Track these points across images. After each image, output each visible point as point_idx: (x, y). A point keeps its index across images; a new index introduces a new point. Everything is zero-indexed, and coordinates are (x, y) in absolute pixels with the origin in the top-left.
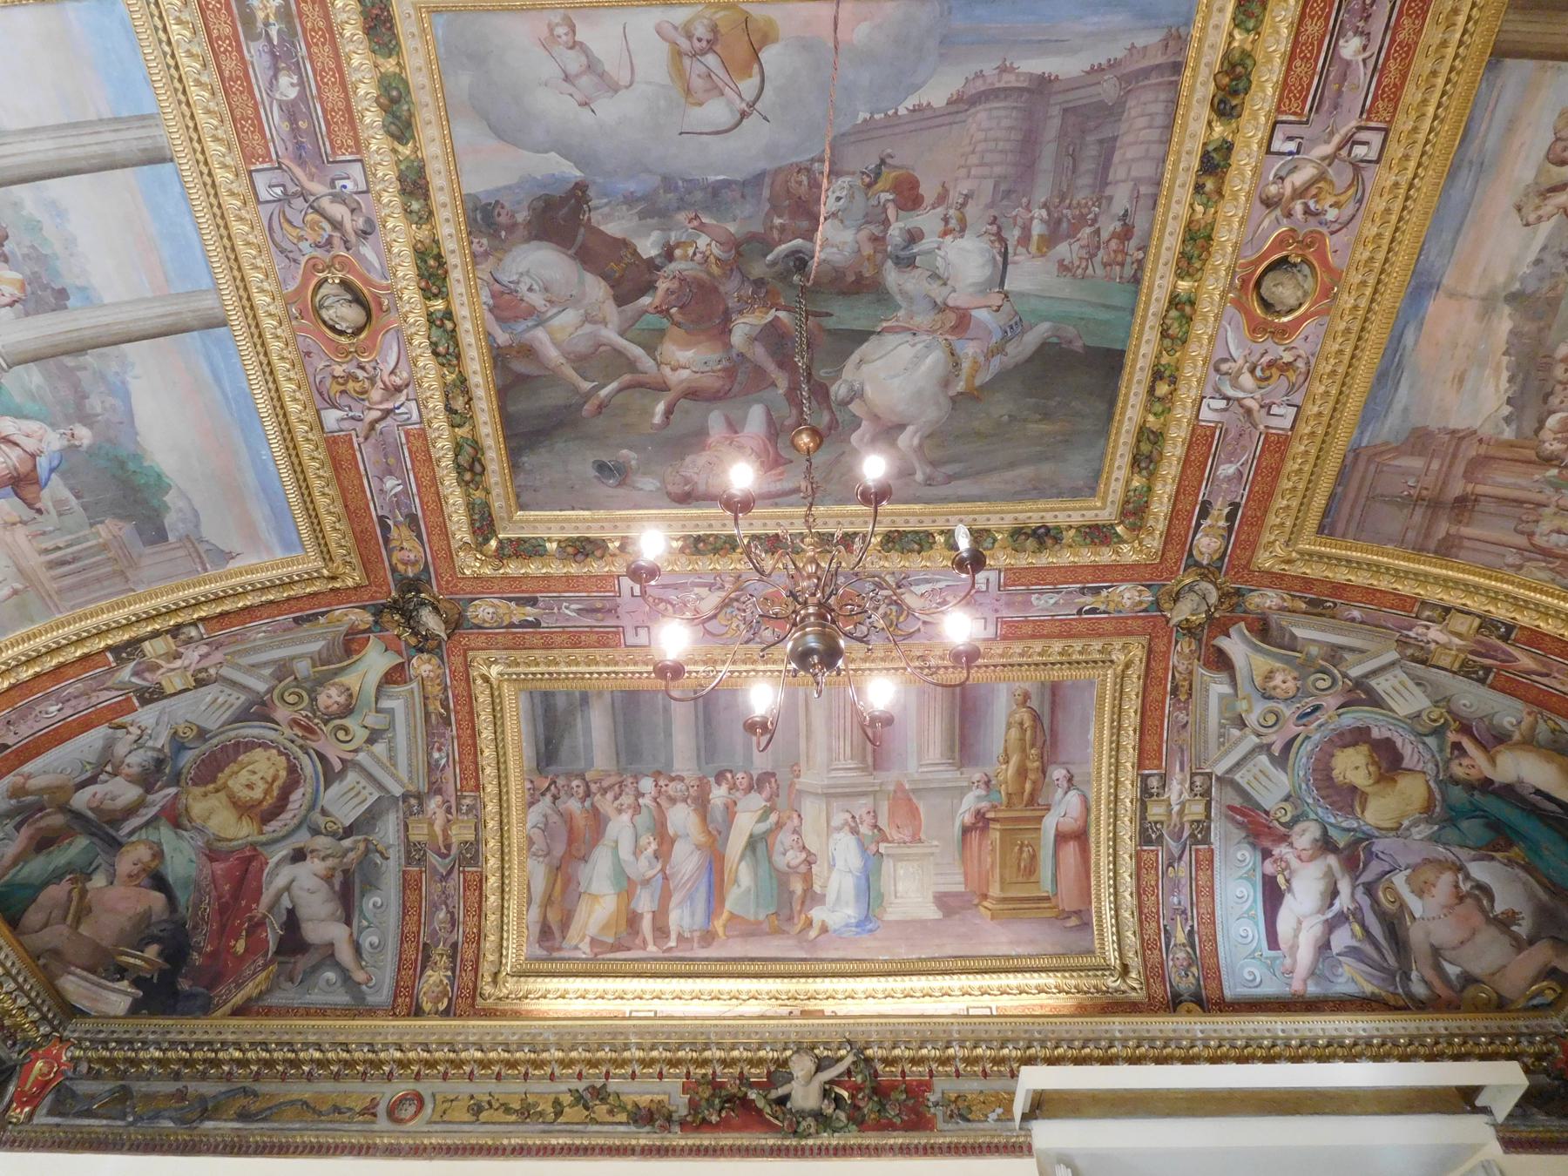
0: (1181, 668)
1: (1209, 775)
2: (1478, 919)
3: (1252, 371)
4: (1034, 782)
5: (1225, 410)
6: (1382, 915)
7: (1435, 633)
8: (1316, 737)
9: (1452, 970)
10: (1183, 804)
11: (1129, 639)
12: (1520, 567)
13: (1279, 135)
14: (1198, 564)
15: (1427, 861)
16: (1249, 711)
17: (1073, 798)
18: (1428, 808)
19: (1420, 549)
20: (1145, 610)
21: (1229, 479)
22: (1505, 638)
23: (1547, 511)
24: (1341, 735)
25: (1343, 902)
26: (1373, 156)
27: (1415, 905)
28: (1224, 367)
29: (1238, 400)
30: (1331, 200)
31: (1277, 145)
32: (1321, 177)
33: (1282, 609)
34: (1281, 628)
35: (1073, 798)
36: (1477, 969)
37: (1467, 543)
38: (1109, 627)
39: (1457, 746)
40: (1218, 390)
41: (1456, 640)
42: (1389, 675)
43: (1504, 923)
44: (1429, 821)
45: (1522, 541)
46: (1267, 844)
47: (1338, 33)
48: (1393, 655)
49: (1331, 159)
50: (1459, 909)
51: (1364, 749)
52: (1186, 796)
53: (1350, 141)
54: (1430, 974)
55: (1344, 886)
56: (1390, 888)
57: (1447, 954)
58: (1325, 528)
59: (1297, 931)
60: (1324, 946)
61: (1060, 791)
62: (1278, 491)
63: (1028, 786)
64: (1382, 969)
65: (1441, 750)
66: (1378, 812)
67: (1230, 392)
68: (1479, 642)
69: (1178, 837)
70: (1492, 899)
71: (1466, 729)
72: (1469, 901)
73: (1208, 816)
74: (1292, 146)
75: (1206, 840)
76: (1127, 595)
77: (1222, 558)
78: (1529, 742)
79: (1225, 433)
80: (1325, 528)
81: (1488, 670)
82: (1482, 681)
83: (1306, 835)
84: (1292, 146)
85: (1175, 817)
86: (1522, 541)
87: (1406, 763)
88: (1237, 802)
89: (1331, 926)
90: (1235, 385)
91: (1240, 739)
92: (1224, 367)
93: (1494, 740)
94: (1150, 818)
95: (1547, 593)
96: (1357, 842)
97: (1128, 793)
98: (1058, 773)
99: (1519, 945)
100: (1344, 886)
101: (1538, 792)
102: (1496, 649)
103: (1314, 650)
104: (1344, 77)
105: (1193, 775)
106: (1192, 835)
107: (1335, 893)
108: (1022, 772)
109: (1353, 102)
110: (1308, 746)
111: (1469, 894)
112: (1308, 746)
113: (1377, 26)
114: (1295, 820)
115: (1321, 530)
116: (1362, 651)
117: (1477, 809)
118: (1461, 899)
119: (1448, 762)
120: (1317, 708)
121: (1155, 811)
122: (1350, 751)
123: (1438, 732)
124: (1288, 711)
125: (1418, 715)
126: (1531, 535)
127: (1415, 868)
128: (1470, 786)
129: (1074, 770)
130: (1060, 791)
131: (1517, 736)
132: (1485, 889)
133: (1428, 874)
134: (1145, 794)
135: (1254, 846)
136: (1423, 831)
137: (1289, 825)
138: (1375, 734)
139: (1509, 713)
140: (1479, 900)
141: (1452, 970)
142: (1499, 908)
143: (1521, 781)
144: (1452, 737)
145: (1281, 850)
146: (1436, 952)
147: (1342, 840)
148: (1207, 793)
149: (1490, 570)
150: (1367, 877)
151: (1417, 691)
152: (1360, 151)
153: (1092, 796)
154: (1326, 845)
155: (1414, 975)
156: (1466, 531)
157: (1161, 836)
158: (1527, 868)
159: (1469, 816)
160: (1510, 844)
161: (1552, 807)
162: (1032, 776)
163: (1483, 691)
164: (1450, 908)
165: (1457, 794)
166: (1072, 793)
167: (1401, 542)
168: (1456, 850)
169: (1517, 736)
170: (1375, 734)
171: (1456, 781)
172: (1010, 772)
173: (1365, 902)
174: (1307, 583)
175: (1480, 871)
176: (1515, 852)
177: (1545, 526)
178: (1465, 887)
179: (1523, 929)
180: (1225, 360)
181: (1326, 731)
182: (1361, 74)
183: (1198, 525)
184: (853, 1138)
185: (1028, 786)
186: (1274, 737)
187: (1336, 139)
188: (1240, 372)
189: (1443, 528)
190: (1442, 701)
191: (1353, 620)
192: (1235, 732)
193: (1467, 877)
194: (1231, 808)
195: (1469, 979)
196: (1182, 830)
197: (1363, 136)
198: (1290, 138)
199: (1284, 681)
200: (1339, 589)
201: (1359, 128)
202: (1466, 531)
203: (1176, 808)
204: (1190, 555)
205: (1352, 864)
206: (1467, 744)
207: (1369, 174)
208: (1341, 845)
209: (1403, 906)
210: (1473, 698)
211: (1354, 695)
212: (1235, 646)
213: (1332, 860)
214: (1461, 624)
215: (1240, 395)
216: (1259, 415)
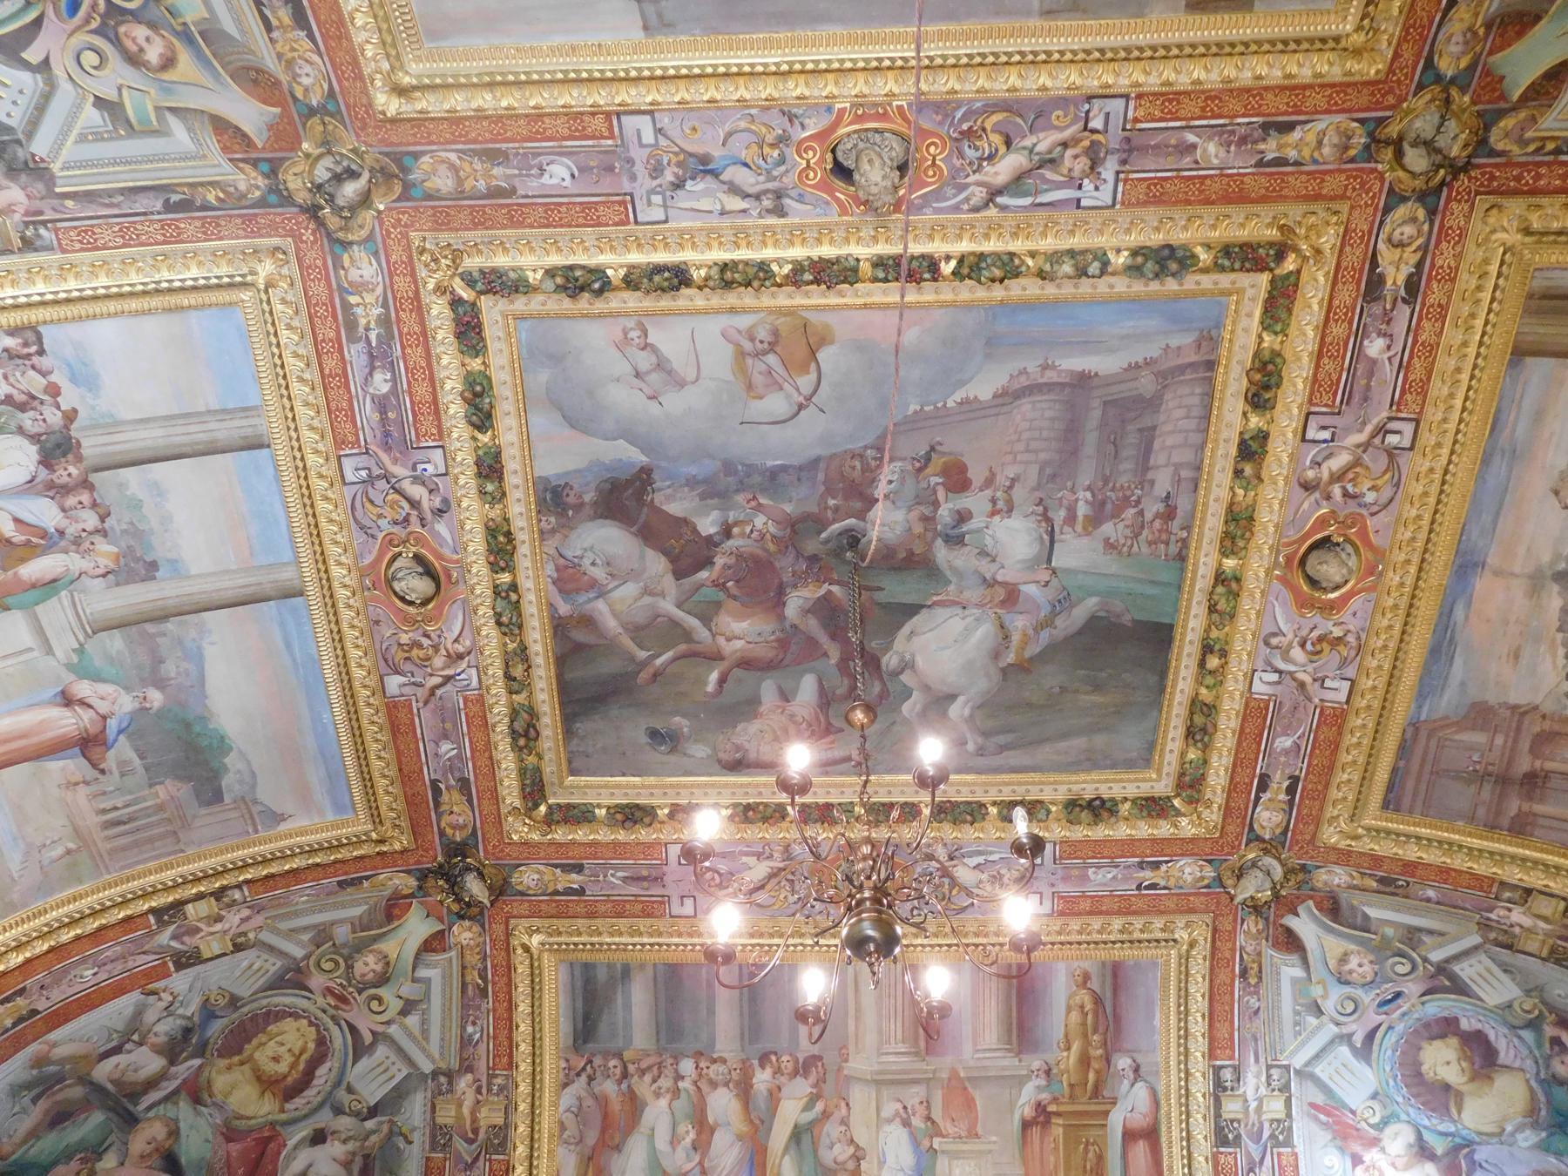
1: (1287, 1068)
3: (1303, 645)
4: (1097, 1072)
5: (1279, 683)
8: (1400, 1028)
10: (1260, 1100)
21: (1286, 752)
24: (1427, 1025)
26: (1406, 443)
28: (1274, 641)
29: (1291, 673)
32: (1357, 462)
34: (1353, 908)
37: (1541, 821)
40: (1269, 664)
41: (1542, 924)
42: (1473, 961)
44: (1535, 1125)
46: (1356, 1147)
47: (1361, 334)
48: (1476, 939)
49: (1366, 446)
52: (1263, 1090)
53: (1382, 431)
63: (1091, 1076)
67: (1282, 666)
73: (1289, 1115)
74: (1326, 435)
75: (1288, 1143)
76: (1188, 870)
79: (1279, 705)
84: (1326, 435)
85: (1253, 1117)
90: (1286, 657)
94: (1225, 1116)
96: (1456, 1149)
98: (1123, 1062)
104: (1370, 374)
105: (1269, 1067)
106: (1272, 1136)
110: (1392, 1038)
112: (1392, 1038)
113: (1400, 326)
115: (1386, 805)
116: (1442, 934)
120: (1398, 995)
121: (1231, 1108)
124: (1368, 998)
129: (1140, 1059)
135: (1342, 1150)
138: (1465, 1025)
148: (1285, 1088)
152: (1392, 439)
153: (1161, 1089)
156: (1539, 808)
157: (1238, 1137)
162: (1095, 1065)
166: (1139, 1085)
167: (1471, 819)
172: (1072, 1060)
180: (1274, 635)
181: (1410, 1021)
183: (1258, 799)
185: (1091, 1076)
186: (1354, 1027)
187: (1369, 428)
188: (1290, 646)
191: (1428, 900)
194: (1313, 1106)
197: (1393, 425)
198: (1324, 428)
199: (1360, 965)
200: (1410, 867)
201: (1390, 419)
202: (1539, 808)
203: (1253, 1105)
207: (1403, 459)
208: (1439, 1152)
212: (1304, 925)
215: (1292, 668)
216: (1314, 688)
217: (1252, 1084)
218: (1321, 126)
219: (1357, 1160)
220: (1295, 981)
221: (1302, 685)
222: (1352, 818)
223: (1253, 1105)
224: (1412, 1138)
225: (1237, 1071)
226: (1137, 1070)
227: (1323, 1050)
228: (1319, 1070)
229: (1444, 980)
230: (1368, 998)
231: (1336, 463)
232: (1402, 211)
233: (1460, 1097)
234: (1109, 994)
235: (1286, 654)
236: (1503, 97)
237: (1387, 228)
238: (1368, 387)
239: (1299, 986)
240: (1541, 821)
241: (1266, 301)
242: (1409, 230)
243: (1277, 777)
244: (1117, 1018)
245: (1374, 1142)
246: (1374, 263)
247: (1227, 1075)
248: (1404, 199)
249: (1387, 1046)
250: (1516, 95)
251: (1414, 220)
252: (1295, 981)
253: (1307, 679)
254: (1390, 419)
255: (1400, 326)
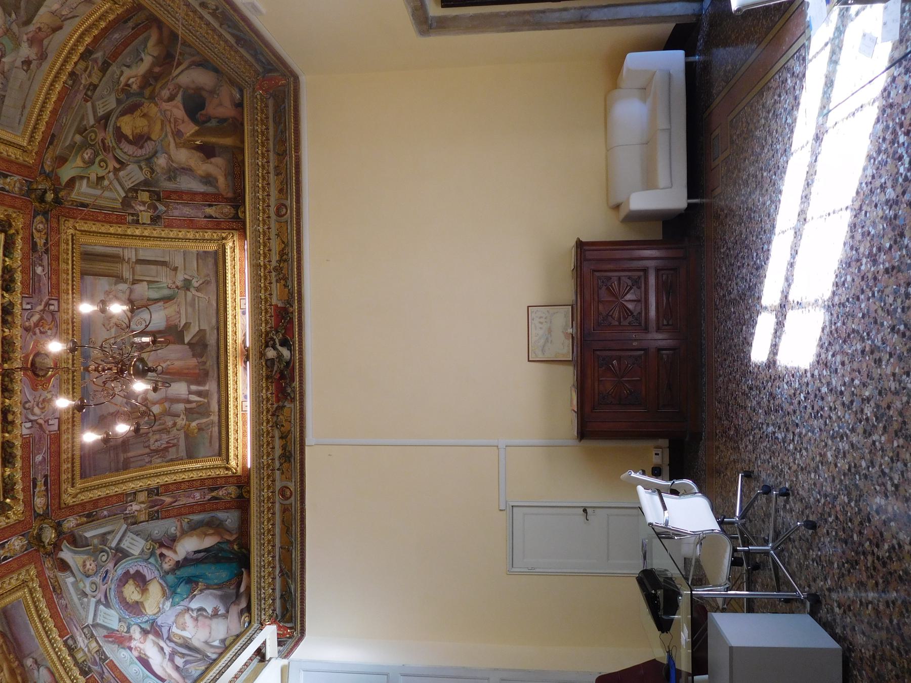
0: (52, 576)
1: (88, 626)
2: (207, 621)
3: (38, 405)
4: (21, 675)
5: (31, 427)
6: (181, 645)
7: (135, 507)
8: (113, 587)
9: (216, 643)
10: (87, 646)
11: (27, 568)
12: (151, 462)
13: (24, 303)
14: (39, 515)
15: (177, 616)
16: (85, 587)
17: (43, 671)
18: (164, 594)
19: (117, 470)
20: (26, 550)
21: (40, 463)
22: (157, 494)
23: (150, 435)
24: (120, 580)
25: (167, 650)
26: (56, 309)
27: (186, 634)
28: (27, 406)
29: (36, 421)
30: (47, 327)
31: (25, 306)
32: (41, 319)
33: (78, 525)
34: (81, 536)
35: (43, 671)
36: (222, 636)
37: (132, 460)
38: (15, 566)
39: (162, 555)
40: (27, 418)
41: (143, 506)
42: (126, 538)
43: (215, 614)
44: (167, 599)
45: (147, 450)
46: (127, 644)
47: (34, 265)
48: (125, 526)
49: (43, 311)
50: (199, 624)
51: (131, 582)
52: (86, 641)
53: (48, 304)
54: (213, 650)
55: (162, 644)
56: (175, 634)
57: (210, 640)
58: (83, 476)
59: (164, 669)
60: (177, 668)
61: (36, 672)
62: (62, 461)
63: (19, 678)
64: (200, 660)
65: (157, 561)
66: (150, 608)
67: (32, 418)
68: (150, 502)
69: (95, 663)
70: (205, 610)
71: (162, 545)
72: (200, 618)
73: (100, 646)
74: (29, 307)
75: (107, 658)
76: (16, 544)
77: (47, 508)
78: (184, 533)
79: (34, 439)
80: (83, 476)
81: (157, 512)
82: (158, 518)
83: (136, 633)
84: (29, 307)
85: (89, 655)
86: (147, 450)
87: (148, 578)
88: (105, 633)
89: (172, 660)
90: (34, 414)
91: (89, 602)
92: (27, 406)
93: (170, 542)
94: (80, 661)
95: (163, 467)
96: (152, 624)
97: (65, 653)
98: (29, 662)
99: (225, 616)
100: (162, 644)
101: (195, 552)
102: (156, 500)
103: (96, 541)
104: (39, 281)
105: (82, 629)
106: (100, 659)
107: (162, 649)
108: (12, 672)
109: (45, 290)
110: (112, 593)
111: (198, 616)
112: (112, 593)
113: (45, 263)
114: (129, 629)
115: (81, 478)
116: (113, 531)
117: (180, 578)
118: (196, 620)
119: (161, 565)
120: (107, 572)
121: (80, 656)
122: (127, 586)
123: (152, 554)
124: (97, 579)
125: (143, 551)
126: (148, 447)
127: (175, 622)
128: (173, 571)
129: (35, 656)
130: (36, 672)
131: (178, 534)
132: (201, 609)
133: (181, 621)
134: (72, 650)
135: (123, 648)
136: (168, 604)
137: (128, 631)
138: (132, 571)
139: (171, 526)
140: (203, 615)
141: (216, 643)
142: (210, 611)
143: (188, 553)
144: (158, 552)
145: (133, 644)
146: (206, 643)
147: (147, 627)
148: (92, 636)
149: (142, 467)
150: (165, 636)
151: (138, 538)
152: (52, 307)
153: (50, 664)
154: (145, 632)
155: (209, 654)
156: (130, 454)
157: (89, 668)
158: (208, 587)
159: (178, 585)
160: (197, 583)
161: (202, 554)
162: (18, 671)
163: (160, 522)
164: (196, 626)
165: (171, 578)
166: (41, 669)
167: (111, 471)
168: (182, 603)
169: (178, 534)
170: (132, 571)
171: (167, 573)
172: (7, 676)
173: (172, 645)
174: (83, 505)
175: (194, 605)
176: (201, 586)
177: (152, 441)
178: (195, 614)
179: (222, 611)
180: (26, 403)
181: (115, 582)
182: (45, 280)
183: (34, 492)
184: (297, 383)
185: (19, 678)
186: (99, 595)
187: (43, 303)
188: (33, 407)
189: (122, 457)
190: (148, 538)
191: (105, 517)
192: (85, 600)
193: (192, 610)
194: (105, 637)
195: (223, 641)
196: (95, 659)
197: (52, 302)
198: (28, 304)
199: (91, 566)
200: (95, 502)
201: (50, 299)
202: (130, 454)
203: (86, 650)
204: (35, 511)
205: (158, 634)
206: (165, 551)
207: (57, 315)
208: (149, 629)
209: (184, 638)
210: (159, 528)
211: (117, 557)
212: (66, 554)
213: (151, 637)
214: (142, 497)
215: (36, 418)
216: (45, 426)
217: (81, 642)
218: (15, 179)
219: (130, 649)
220: (73, 584)
221: (40, 425)
222: (73, 486)
223: (86, 650)
224: (139, 630)
225: (72, 637)
226: (36, 662)
227: (95, 611)
228: (100, 621)
229: (121, 554)
230: (97, 579)
231: (36, 318)
232: (39, 218)
233: (142, 603)
234: (7, 629)
235: (31, 410)
236: (60, 184)
237: (35, 224)
238: (40, 287)
239: (75, 584)
240: (132, 460)
241: (4, 246)
242: (41, 226)
243: (39, 478)
244: (16, 639)
245: (131, 638)
246: (33, 238)
247: (70, 642)
248: (39, 214)
249: (113, 600)
250: (63, 184)
251: (42, 222)
252: (73, 584)
253: (41, 421)
254: (50, 299)
255: (45, 263)
